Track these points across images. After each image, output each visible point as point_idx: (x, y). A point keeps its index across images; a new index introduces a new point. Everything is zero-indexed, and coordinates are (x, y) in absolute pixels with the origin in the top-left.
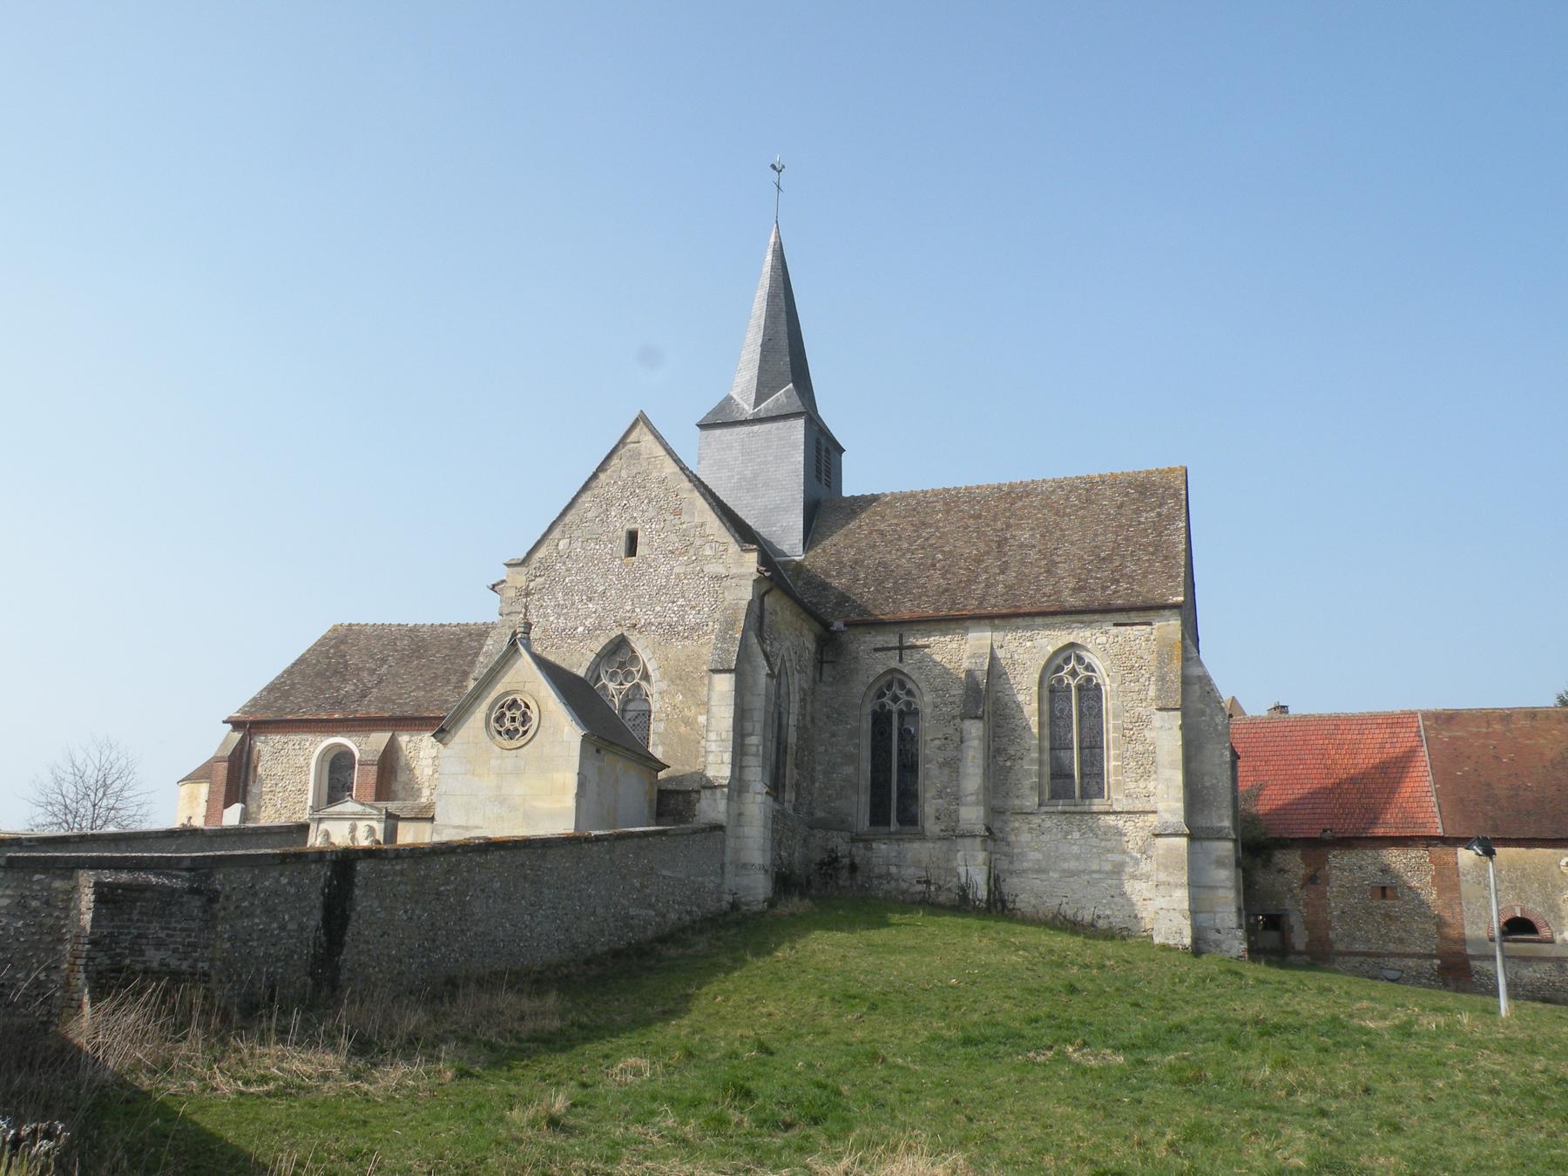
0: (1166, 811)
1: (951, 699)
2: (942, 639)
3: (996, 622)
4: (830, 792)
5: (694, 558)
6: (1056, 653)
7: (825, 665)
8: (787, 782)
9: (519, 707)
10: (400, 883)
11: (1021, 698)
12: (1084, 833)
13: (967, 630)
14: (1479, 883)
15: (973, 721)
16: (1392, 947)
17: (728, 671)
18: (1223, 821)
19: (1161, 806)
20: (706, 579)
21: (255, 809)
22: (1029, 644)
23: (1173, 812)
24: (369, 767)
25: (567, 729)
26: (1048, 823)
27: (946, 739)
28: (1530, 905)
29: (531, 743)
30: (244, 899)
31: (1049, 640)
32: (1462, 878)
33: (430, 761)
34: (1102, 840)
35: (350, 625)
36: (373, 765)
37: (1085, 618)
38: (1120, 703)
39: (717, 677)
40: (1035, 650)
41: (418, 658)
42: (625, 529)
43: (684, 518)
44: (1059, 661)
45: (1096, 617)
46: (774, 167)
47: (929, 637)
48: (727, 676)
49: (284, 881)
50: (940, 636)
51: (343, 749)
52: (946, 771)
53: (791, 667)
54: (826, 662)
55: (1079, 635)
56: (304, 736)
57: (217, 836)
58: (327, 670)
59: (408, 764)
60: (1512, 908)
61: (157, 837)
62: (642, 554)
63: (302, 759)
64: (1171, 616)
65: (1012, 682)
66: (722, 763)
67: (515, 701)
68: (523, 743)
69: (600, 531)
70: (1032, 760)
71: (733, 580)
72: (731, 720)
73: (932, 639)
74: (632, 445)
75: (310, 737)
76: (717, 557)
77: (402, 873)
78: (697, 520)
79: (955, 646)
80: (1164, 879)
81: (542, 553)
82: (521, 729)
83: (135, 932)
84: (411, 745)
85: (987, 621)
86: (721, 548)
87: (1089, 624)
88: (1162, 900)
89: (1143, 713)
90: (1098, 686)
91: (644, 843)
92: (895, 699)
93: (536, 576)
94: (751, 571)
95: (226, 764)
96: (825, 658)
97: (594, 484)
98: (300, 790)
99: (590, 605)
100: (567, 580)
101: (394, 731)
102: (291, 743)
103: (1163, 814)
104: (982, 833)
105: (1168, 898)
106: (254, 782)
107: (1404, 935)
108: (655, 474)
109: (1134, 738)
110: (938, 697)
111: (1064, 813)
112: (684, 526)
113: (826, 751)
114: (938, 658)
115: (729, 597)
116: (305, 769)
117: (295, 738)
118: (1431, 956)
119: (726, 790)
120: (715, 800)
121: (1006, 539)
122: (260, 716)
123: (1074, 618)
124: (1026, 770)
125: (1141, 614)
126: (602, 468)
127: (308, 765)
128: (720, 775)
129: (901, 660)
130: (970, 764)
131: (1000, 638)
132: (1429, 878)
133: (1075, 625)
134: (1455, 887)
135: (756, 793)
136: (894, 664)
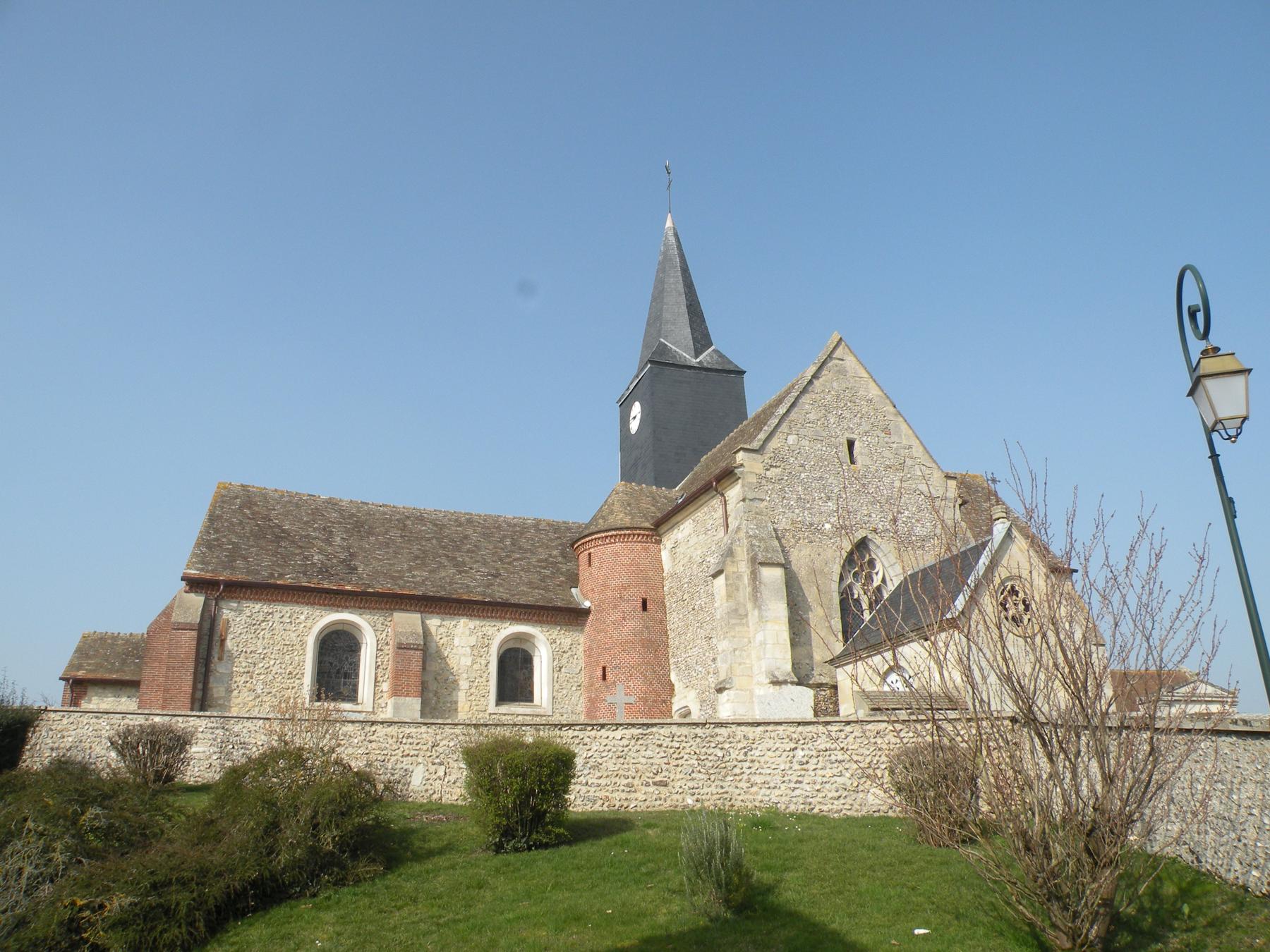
21: (223, 694)
24: (412, 652)
33: (468, 650)
36: (416, 649)
56: (297, 608)
59: (438, 652)
63: (294, 635)
74: (837, 361)
75: (306, 610)
78: (905, 442)
83: (329, 840)
84: (442, 630)
93: (771, 466)
97: (810, 389)
98: (290, 673)
99: (830, 504)
100: (803, 475)
102: (277, 616)
106: (220, 659)
112: (895, 445)
116: (298, 647)
117: (283, 611)
127: (303, 643)
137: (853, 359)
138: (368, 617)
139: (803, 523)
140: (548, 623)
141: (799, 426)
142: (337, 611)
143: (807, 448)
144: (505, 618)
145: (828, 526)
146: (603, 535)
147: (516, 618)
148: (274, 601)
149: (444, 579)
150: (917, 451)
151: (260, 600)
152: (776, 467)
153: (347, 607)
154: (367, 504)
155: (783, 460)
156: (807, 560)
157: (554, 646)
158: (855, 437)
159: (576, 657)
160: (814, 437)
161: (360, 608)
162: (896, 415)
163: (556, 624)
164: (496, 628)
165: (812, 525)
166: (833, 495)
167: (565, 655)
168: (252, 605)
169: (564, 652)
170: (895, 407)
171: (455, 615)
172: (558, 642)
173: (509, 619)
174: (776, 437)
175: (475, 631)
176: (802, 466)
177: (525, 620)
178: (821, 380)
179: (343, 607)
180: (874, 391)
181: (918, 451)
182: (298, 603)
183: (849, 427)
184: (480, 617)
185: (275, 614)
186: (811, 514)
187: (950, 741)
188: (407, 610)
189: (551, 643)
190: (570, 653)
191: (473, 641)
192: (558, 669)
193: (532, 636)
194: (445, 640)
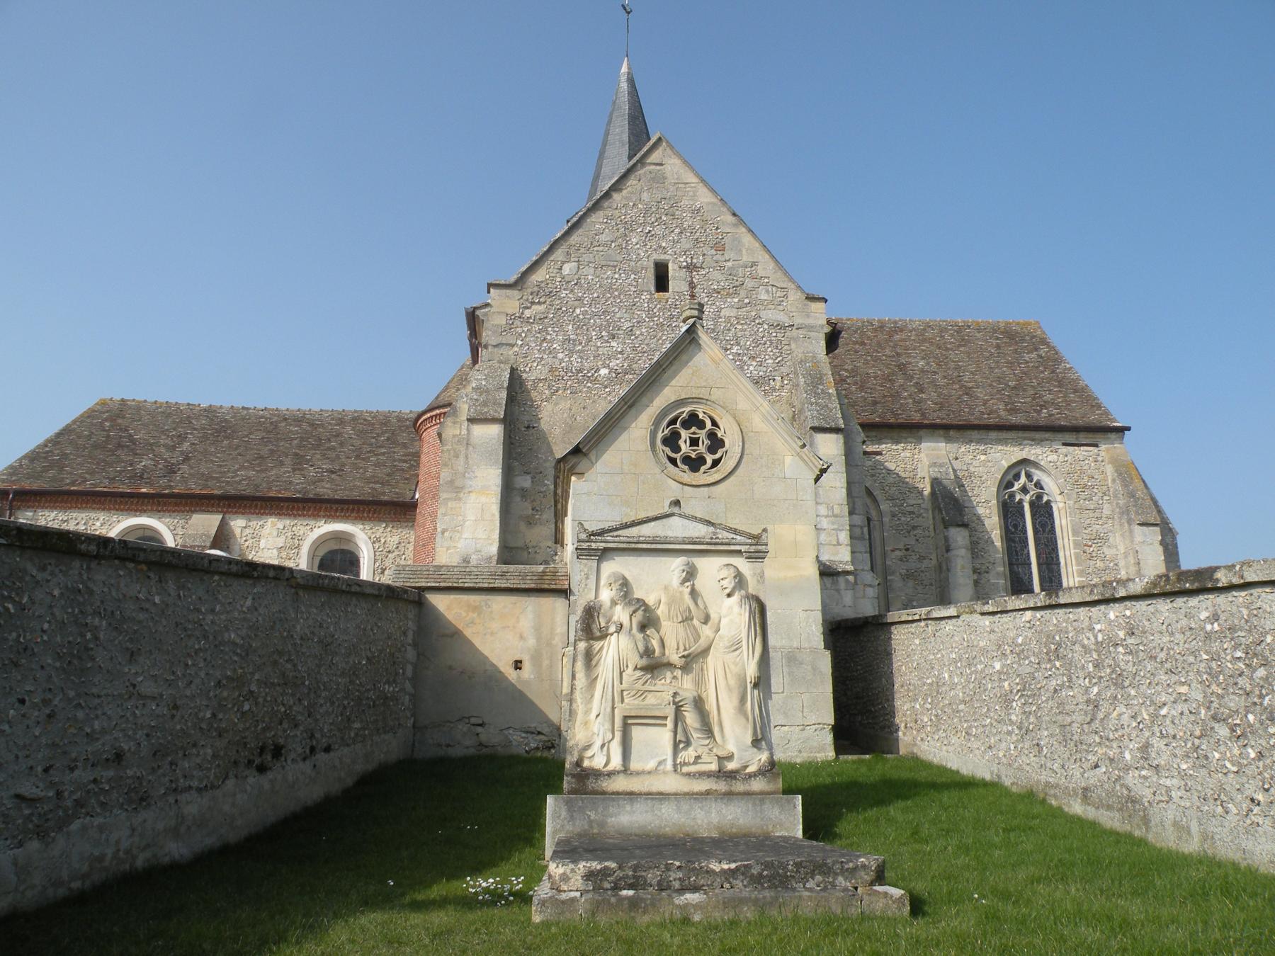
1: (909, 509)
2: (894, 447)
3: (952, 433)
5: (747, 301)
9: (701, 425)
11: (981, 511)
13: (920, 440)
15: (958, 529)
22: (983, 457)
25: (788, 460)
27: (907, 550)
29: (732, 478)
31: (1003, 455)
33: (275, 552)
35: (123, 400)
37: (1038, 435)
38: (1077, 520)
39: (820, 438)
40: (990, 464)
41: (227, 438)
42: (652, 259)
44: (1010, 477)
45: (1047, 435)
47: (880, 444)
48: (833, 437)
50: (893, 443)
51: (148, 533)
52: (911, 583)
55: (1031, 452)
56: (93, 515)
61: (228, 574)
62: (677, 289)
64: (1115, 440)
65: (970, 494)
66: (839, 544)
69: (619, 258)
70: (998, 574)
71: (800, 331)
73: (884, 446)
76: (776, 304)
78: (746, 258)
79: (908, 455)
81: (540, 275)
82: (709, 459)
84: (248, 531)
85: (941, 432)
87: (1039, 442)
89: (1101, 530)
90: (1048, 502)
93: (533, 303)
97: (606, 204)
99: (614, 344)
100: (578, 311)
101: (225, 513)
108: (685, 202)
109: (1094, 554)
110: (894, 506)
112: (730, 264)
114: (891, 466)
115: (798, 350)
119: (851, 578)
120: (838, 591)
122: (27, 485)
123: (1027, 434)
124: (993, 585)
125: (1090, 435)
130: (960, 574)
131: (954, 450)
133: (1026, 442)
135: (865, 585)
137: (677, 161)
138: (168, 520)
139: (567, 370)
140: (370, 520)
141: (582, 250)
142: (136, 516)
143: (590, 277)
144: (319, 516)
145: (604, 372)
146: (429, 415)
147: (331, 515)
148: (70, 508)
149: (241, 478)
150: (764, 269)
151: (56, 508)
152: (539, 303)
153: (145, 511)
154: (248, 409)
155: (549, 295)
156: (565, 415)
157: (377, 545)
158: (667, 257)
159: (404, 557)
160: (604, 263)
161: (159, 511)
162: (735, 225)
163: (380, 520)
164: (308, 528)
165: (580, 371)
166: (621, 332)
167: (390, 555)
168: (47, 514)
169: (389, 552)
170: (734, 215)
171: (262, 514)
172: (383, 541)
173: (324, 517)
174: (544, 267)
175: (284, 532)
176: (579, 299)
177: (342, 517)
178: (624, 192)
179: (141, 511)
180: (704, 197)
181: (766, 267)
182: (94, 509)
183: (660, 247)
184: (290, 515)
185: (70, 521)
186: (582, 358)
187: (247, 598)
188: (208, 511)
189: (374, 542)
190: (396, 553)
191: (280, 542)
192: (380, 571)
193: (353, 536)
194: (250, 541)
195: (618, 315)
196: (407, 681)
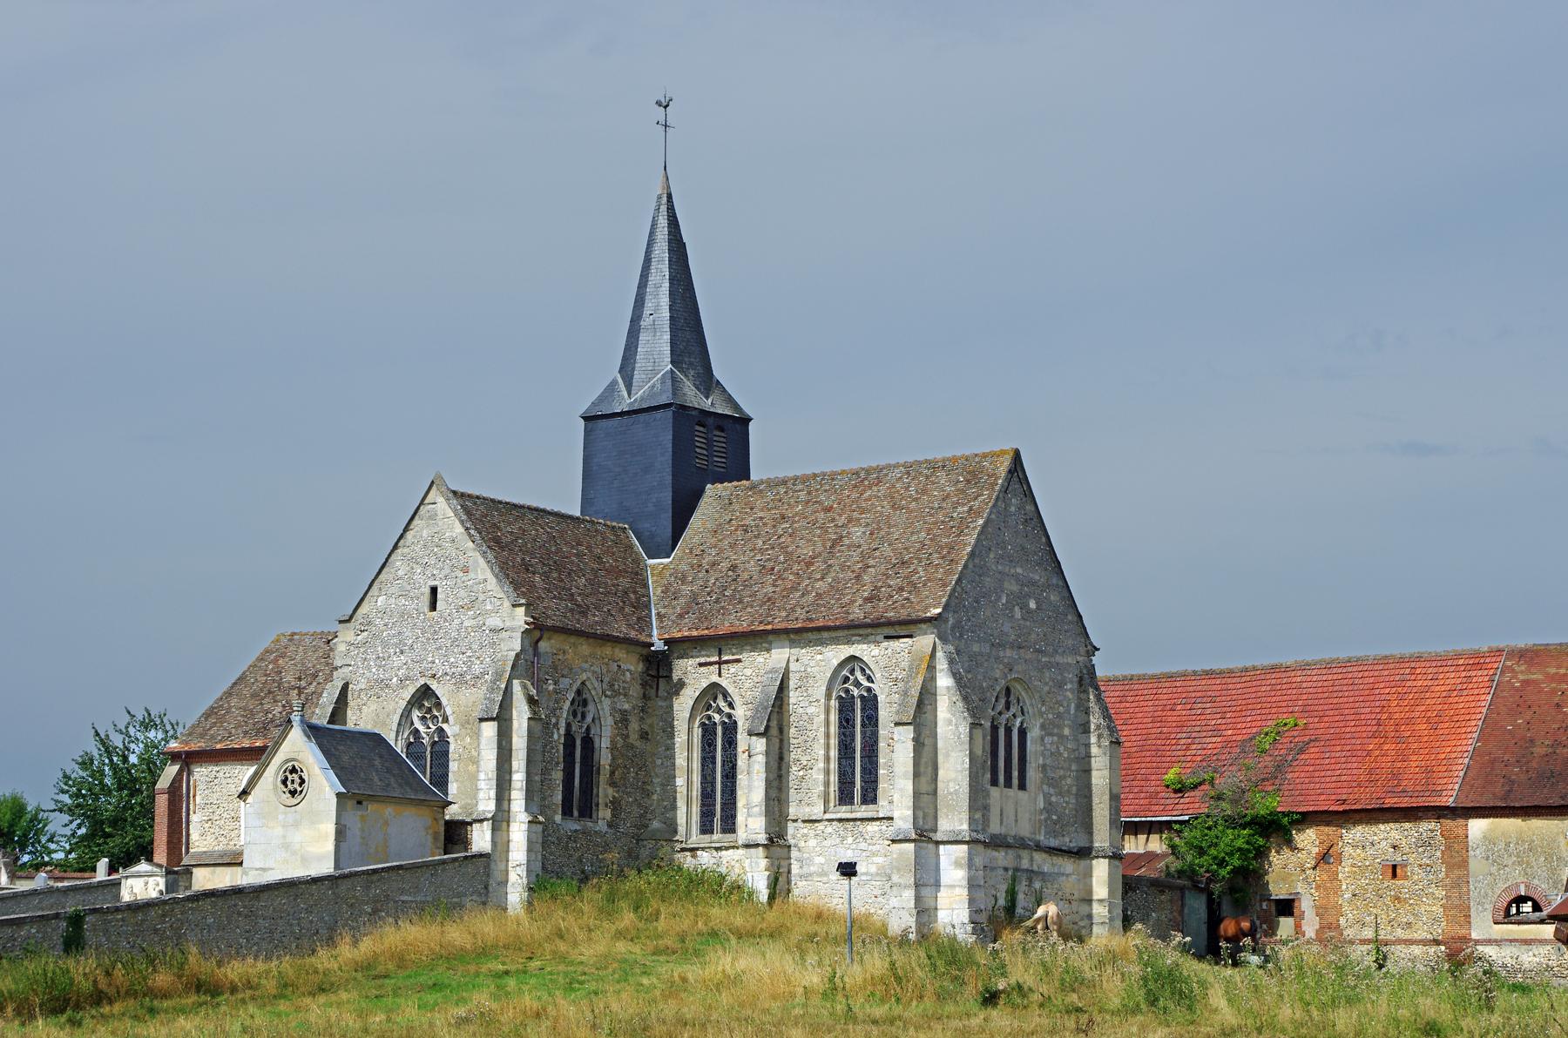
0: (900, 818)
4: (665, 803)
5: (478, 612)
6: (842, 665)
7: (661, 679)
8: (600, 801)
9: (296, 772)
10: (122, 926)
12: (856, 838)
14: (1487, 859)
16: (1400, 933)
17: (492, 719)
18: (962, 824)
19: (896, 815)
20: (487, 631)
23: (903, 819)
26: (829, 829)
28: (1536, 882)
30: (7, 943)
31: (834, 654)
32: (1471, 853)
34: (869, 844)
39: (485, 725)
43: (471, 575)
46: (659, 103)
49: (33, 931)
53: (597, 694)
54: (662, 677)
55: (859, 650)
57: (71, 890)
58: (262, 690)
60: (1517, 885)
66: (489, 799)
67: (294, 767)
68: (300, 800)
70: (819, 769)
72: (495, 761)
77: (123, 920)
78: (481, 577)
80: (897, 881)
86: (498, 603)
88: (895, 900)
91: (375, 877)
92: (857, 684)
94: (520, 624)
95: (166, 796)
96: (661, 674)
99: (402, 658)
102: (222, 772)
103: (898, 821)
104: (763, 843)
105: (899, 898)
107: (1412, 919)
111: (840, 820)
113: (662, 764)
118: (1437, 942)
120: (483, 831)
121: (842, 537)
126: (406, 529)
128: (487, 809)
129: (720, 675)
132: (1439, 854)
133: (854, 638)
134: (1464, 864)
136: (715, 678)
160: (400, 593)
195: (406, 635)
196: (1041, 795)
